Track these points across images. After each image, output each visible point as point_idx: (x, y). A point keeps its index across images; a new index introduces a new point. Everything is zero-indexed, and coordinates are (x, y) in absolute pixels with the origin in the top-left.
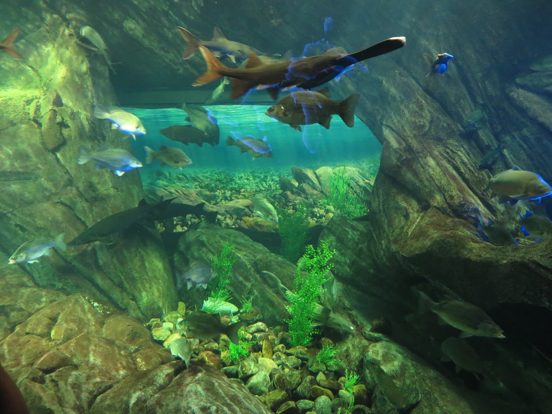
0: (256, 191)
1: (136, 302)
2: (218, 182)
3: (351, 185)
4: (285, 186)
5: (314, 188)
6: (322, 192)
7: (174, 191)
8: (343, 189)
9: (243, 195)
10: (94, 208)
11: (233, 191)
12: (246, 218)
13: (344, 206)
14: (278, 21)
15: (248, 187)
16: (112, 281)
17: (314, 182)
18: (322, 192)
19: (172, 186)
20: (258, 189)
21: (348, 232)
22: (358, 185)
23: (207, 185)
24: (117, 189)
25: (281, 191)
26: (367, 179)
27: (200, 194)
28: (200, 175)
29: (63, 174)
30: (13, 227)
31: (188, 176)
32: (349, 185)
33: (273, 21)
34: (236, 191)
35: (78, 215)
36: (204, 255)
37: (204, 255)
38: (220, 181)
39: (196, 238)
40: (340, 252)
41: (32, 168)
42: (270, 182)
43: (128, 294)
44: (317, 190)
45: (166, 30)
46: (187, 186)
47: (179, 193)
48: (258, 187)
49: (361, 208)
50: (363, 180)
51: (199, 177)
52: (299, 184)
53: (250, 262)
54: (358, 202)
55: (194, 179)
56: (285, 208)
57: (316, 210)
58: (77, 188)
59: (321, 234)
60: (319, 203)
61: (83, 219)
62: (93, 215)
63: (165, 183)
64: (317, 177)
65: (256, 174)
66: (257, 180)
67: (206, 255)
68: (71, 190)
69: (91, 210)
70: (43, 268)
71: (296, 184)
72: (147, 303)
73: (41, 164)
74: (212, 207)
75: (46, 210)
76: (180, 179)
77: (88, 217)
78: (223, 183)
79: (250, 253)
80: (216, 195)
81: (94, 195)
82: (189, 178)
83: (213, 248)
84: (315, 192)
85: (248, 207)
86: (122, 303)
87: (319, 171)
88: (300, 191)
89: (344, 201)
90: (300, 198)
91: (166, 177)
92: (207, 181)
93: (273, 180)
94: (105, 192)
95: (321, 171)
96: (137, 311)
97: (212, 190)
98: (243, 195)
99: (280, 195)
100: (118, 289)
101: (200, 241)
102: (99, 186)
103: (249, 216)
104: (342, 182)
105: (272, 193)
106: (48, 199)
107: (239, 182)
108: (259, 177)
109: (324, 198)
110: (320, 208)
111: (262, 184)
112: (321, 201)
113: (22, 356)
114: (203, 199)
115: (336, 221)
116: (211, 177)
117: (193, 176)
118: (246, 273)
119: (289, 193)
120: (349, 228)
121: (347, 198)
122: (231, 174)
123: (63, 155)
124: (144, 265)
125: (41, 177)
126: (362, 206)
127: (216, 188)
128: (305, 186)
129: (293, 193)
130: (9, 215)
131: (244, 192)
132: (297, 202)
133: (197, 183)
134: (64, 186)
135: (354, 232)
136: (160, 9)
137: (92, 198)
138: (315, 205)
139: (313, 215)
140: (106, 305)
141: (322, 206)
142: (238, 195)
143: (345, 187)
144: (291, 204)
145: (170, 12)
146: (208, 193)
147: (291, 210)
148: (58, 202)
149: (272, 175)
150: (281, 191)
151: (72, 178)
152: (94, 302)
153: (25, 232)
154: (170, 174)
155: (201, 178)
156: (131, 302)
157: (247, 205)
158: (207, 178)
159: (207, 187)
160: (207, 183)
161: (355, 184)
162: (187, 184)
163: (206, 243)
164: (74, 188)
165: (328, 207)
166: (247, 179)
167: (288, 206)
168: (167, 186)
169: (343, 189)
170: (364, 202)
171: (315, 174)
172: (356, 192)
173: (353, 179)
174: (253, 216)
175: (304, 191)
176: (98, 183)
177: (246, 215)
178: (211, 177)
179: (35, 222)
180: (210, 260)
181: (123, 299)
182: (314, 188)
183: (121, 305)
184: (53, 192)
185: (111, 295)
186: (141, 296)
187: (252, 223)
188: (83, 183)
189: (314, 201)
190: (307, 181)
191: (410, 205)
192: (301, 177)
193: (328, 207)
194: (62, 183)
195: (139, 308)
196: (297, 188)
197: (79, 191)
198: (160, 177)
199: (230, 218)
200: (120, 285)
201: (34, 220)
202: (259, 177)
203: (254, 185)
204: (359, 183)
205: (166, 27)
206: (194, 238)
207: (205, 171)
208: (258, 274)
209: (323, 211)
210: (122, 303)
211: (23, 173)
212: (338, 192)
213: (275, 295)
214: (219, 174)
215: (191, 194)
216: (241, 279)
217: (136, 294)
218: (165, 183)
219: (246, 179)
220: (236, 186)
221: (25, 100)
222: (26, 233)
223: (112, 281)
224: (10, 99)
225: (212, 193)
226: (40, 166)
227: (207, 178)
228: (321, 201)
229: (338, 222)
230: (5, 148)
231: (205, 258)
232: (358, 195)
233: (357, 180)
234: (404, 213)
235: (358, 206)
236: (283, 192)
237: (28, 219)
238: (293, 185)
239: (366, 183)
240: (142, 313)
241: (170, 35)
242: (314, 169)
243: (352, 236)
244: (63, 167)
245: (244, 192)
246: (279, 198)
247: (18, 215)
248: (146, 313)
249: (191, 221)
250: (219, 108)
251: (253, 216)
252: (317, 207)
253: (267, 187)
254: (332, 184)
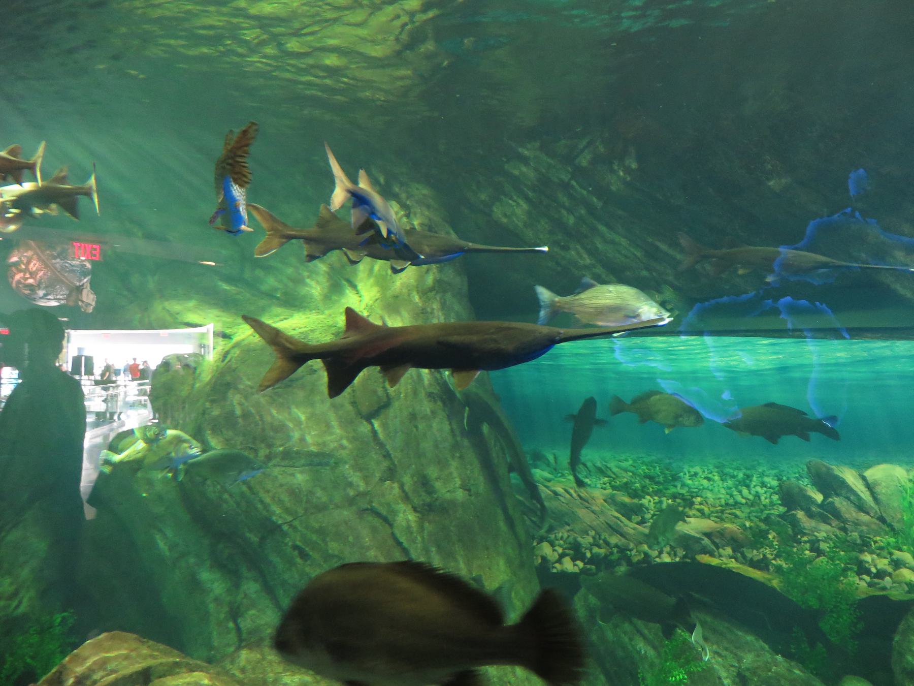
0: (727, 504)
2: (647, 481)
4: (791, 498)
6: (882, 520)
9: (699, 510)
10: (427, 525)
11: (678, 501)
14: (784, 181)
15: (709, 495)
17: (862, 495)
19: (559, 482)
20: (731, 501)
23: (626, 484)
24: (469, 490)
25: (782, 509)
27: (611, 500)
28: (612, 465)
29: (381, 459)
30: (289, 550)
31: (589, 464)
33: (771, 183)
34: (684, 500)
36: (626, 640)
37: (626, 640)
38: (651, 478)
41: (332, 445)
42: (759, 489)
44: (868, 513)
45: (564, 212)
47: (571, 495)
48: (732, 496)
52: (826, 497)
55: (601, 472)
57: (867, 557)
59: (901, 627)
60: (875, 542)
61: (406, 544)
63: (547, 475)
64: (869, 487)
65: (727, 470)
66: (730, 483)
67: (631, 640)
68: (392, 488)
71: (819, 498)
73: (348, 440)
77: (414, 541)
78: (658, 483)
79: (726, 649)
80: (642, 505)
82: (592, 469)
84: (864, 518)
85: (708, 535)
87: (873, 474)
90: (828, 527)
91: (548, 465)
92: (626, 478)
93: (763, 485)
94: (448, 496)
95: (878, 473)
97: (635, 494)
98: (699, 510)
99: (781, 516)
102: (438, 485)
105: (762, 511)
106: (351, 502)
107: (690, 482)
108: (733, 477)
109: (886, 533)
110: (878, 555)
111: (740, 492)
112: (882, 540)
114: (617, 511)
116: (633, 469)
117: (599, 464)
119: (800, 514)
122: (674, 465)
123: (384, 426)
125: (346, 463)
129: (810, 515)
130: (285, 528)
131: (701, 504)
132: (822, 535)
133: (606, 479)
134: (381, 479)
136: (556, 180)
138: (865, 545)
139: (862, 569)
141: (880, 551)
144: (805, 539)
145: (573, 183)
148: (367, 509)
149: (762, 475)
150: (782, 509)
153: (306, 561)
154: (555, 458)
155: (615, 470)
157: (708, 531)
158: (626, 470)
159: (626, 487)
160: (625, 480)
164: (396, 485)
165: (897, 554)
166: (709, 479)
167: (799, 542)
168: (549, 480)
171: (864, 479)
174: (720, 556)
175: (837, 514)
176: (438, 479)
178: (633, 469)
180: (639, 652)
182: (861, 507)
184: (361, 489)
188: (412, 476)
190: (843, 492)
192: (830, 484)
193: (897, 554)
194: (378, 475)
196: (821, 506)
197: (404, 491)
198: (539, 463)
199: (669, 554)
201: (324, 540)
202: (733, 477)
203: (723, 491)
205: (565, 208)
207: (623, 457)
209: (886, 561)
211: (317, 455)
214: (650, 464)
215: (593, 498)
218: (547, 475)
219: (705, 478)
220: (684, 491)
221: (334, 332)
222: (309, 562)
224: (312, 331)
225: (636, 501)
226: (345, 442)
227: (626, 470)
228: (882, 540)
230: (296, 410)
237: (314, 537)
238: (810, 498)
241: (571, 220)
242: (861, 468)
244: (381, 445)
245: (701, 504)
247: (299, 528)
249: (591, 550)
250: (653, 342)
251: (720, 556)
252: (872, 553)
253: (751, 497)
254: (906, 504)
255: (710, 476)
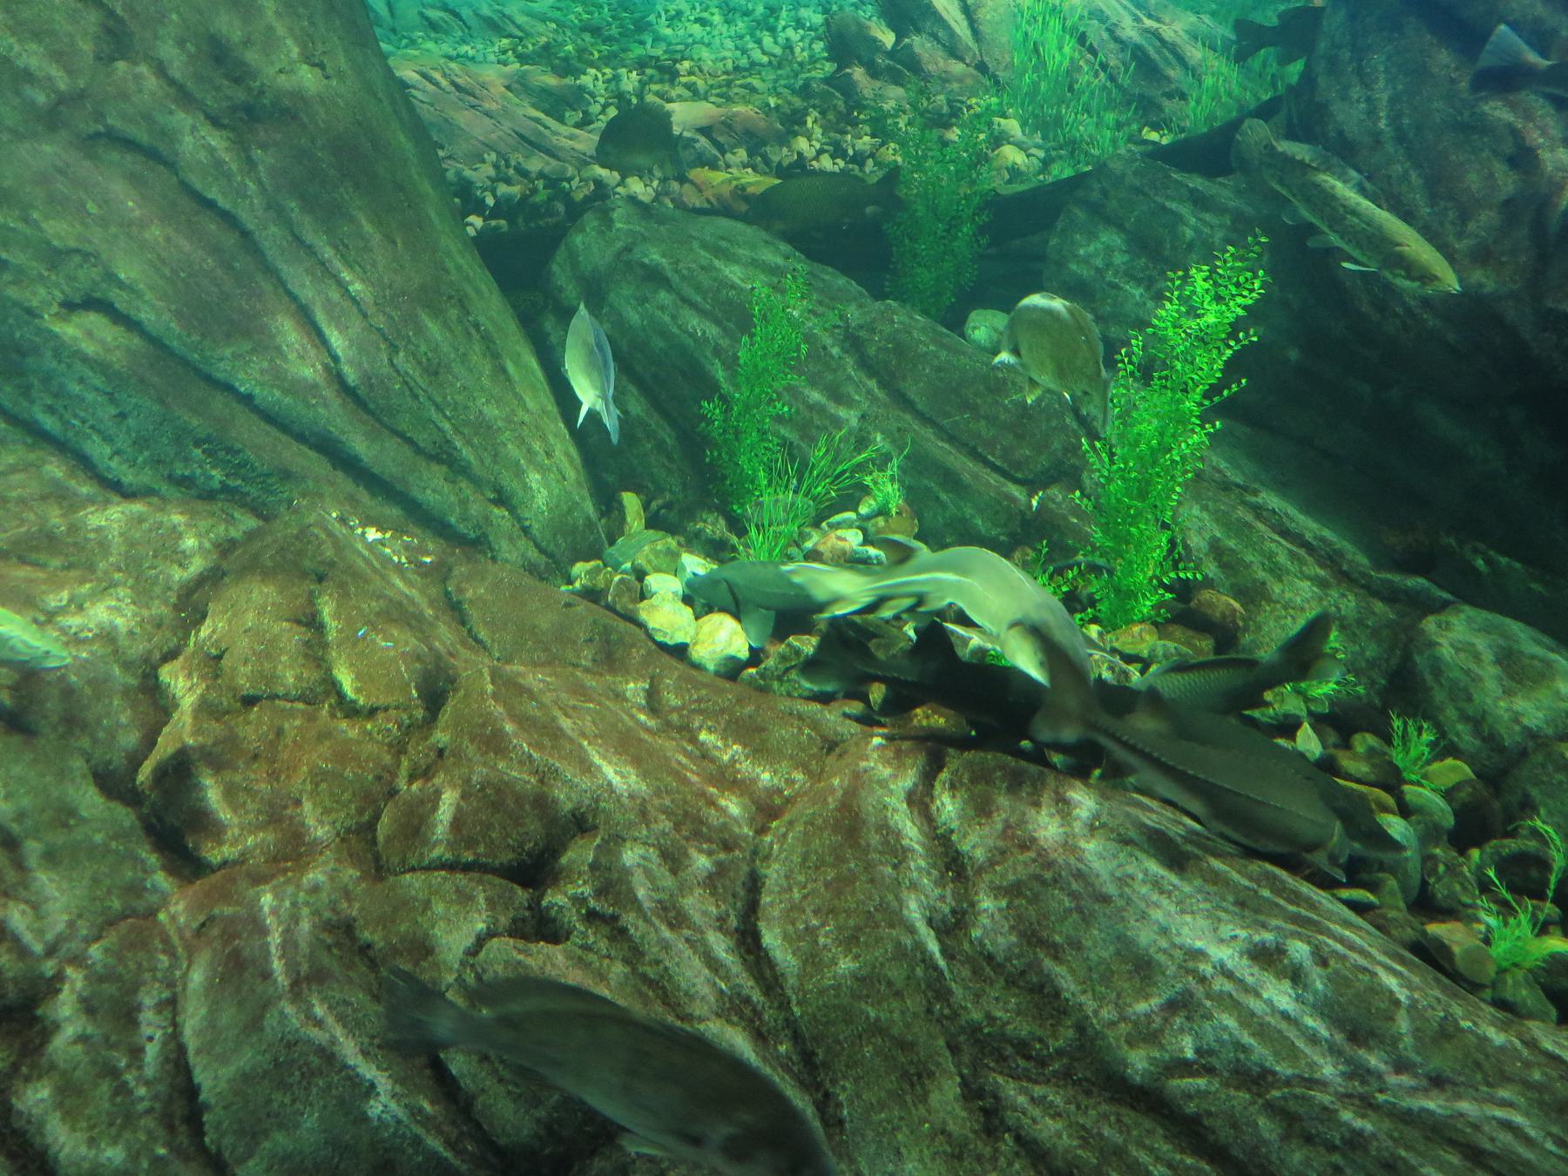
0: (737, 69)
1: (512, 510)
2: (587, 37)
3: (1092, 39)
5: (954, 52)
7: (417, 77)
8: (1060, 53)
9: (688, 86)
11: (649, 71)
12: (700, 174)
13: (1058, 121)
15: (705, 53)
16: (410, 442)
17: (958, 30)
18: (982, 67)
20: (744, 62)
21: (1180, 219)
22: (1117, 40)
23: (546, 47)
24: (321, 66)
25: (829, 67)
26: (1150, 16)
27: (519, 85)
31: (466, 13)
32: (1082, 39)
35: (198, 186)
36: (667, 319)
37: (667, 319)
38: (595, 31)
39: (618, 255)
40: (1148, 288)
42: (790, 33)
43: (476, 482)
44: (961, 59)
46: (465, 56)
47: (437, 84)
48: (744, 51)
49: (1119, 126)
50: (1137, 20)
51: (509, 18)
53: (832, 335)
54: (1110, 105)
56: (845, 133)
58: (161, 69)
60: (970, 107)
61: (222, 203)
62: (259, 182)
67: (674, 317)
69: (251, 164)
70: (122, 416)
71: (888, 38)
72: (550, 510)
74: (571, 137)
75: (60, 171)
76: (433, 26)
77: (241, 192)
78: (608, 40)
80: (582, 89)
81: (240, 96)
82: (473, 22)
83: (698, 288)
84: (957, 68)
85: (705, 131)
86: (464, 518)
88: (904, 66)
89: (1061, 101)
90: (900, 91)
92: (544, 34)
93: (799, 24)
96: (522, 543)
97: (566, 68)
98: (688, 86)
99: (828, 81)
100: (435, 468)
101: (643, 265)
102: (252, 57)
103: (713, 166)
104: (1058, 27)
107: (668, 31)
109: (987, 91)
112: (978, 103)
113: (298, 803)
114: (535, 106)
115: (1123, 176)
118: (829, 377)
119: (858, 73)
120: (1181, 200)
121: (1071, 89)
124: (504, 371)
126: (1123, 118)
127: (580, 59)
128: (920, 44)
129: (874, 72)
132: (889, 106)
134: (98, 58)
135: (1207, 217)
137: (234, 109)
140: (407, 533)
142: (667, 87)
143: (1067, 49)
146: (551, 81)
147: (867, 138)
148: (98, 135)
150: (829, 67)
151: (118, 20)
152: (364, 525)
155: (521, 19)
156: (496, 511)
157: (703, 123)
158: (544, 19)
159: (546, 54)
160: (544, 40)
161: (1105, 35)
162: (465, 49)
163: (669, 274)
164: (143, 69)
166: (702, 22)
169: (1060, 53)
170: (1129, 103)
172: (1104, 67)
173: (1098, 15)
174: (728, 166)
176: (247, 42)
177: (704, 161)
179: (35, 225)
180: (693, 335)
181: (464, 503)
182: (954, 52)
183: (462, 528)
185: (416, 493)
186: (526, 488)
187: (726, 191)
188: (181, 43)
189: (949, 102)
191: (1529, 117)
194: (86, 47)
195: (526, 531)
196: (891, 54)
197: (172, 82)
200: (444, 456)
202: (746, 13)
203: (729, 44)
204: (1119, 33)
206: (609, 254)
208: (870, 378)
210: (464, 518)
212: (1042, 64)
213: (946, 446)
215: (483, 86)
216: (816, 396)
217: (508, 481)
219: (697, 20)
220: (658, 52)
223: (410, 442)
225: (569, 80)
227: (544, 19)
229: (1131, 180)
231: (675, 330)
232: (1112, 78)
233: (1114, 20)
234: (1508, 148)
235: (1110, 117)
236: (839, 69)
238: (875, 40)
239: (1147, 30)
240: (537, 546)
243: (1196, 230)
245: (691, 73)
246: (825, 96)
248: (551, 547)
251: (728, 166)
253: (778, 51)
254: (1019, 36)
255: (705, 15)
